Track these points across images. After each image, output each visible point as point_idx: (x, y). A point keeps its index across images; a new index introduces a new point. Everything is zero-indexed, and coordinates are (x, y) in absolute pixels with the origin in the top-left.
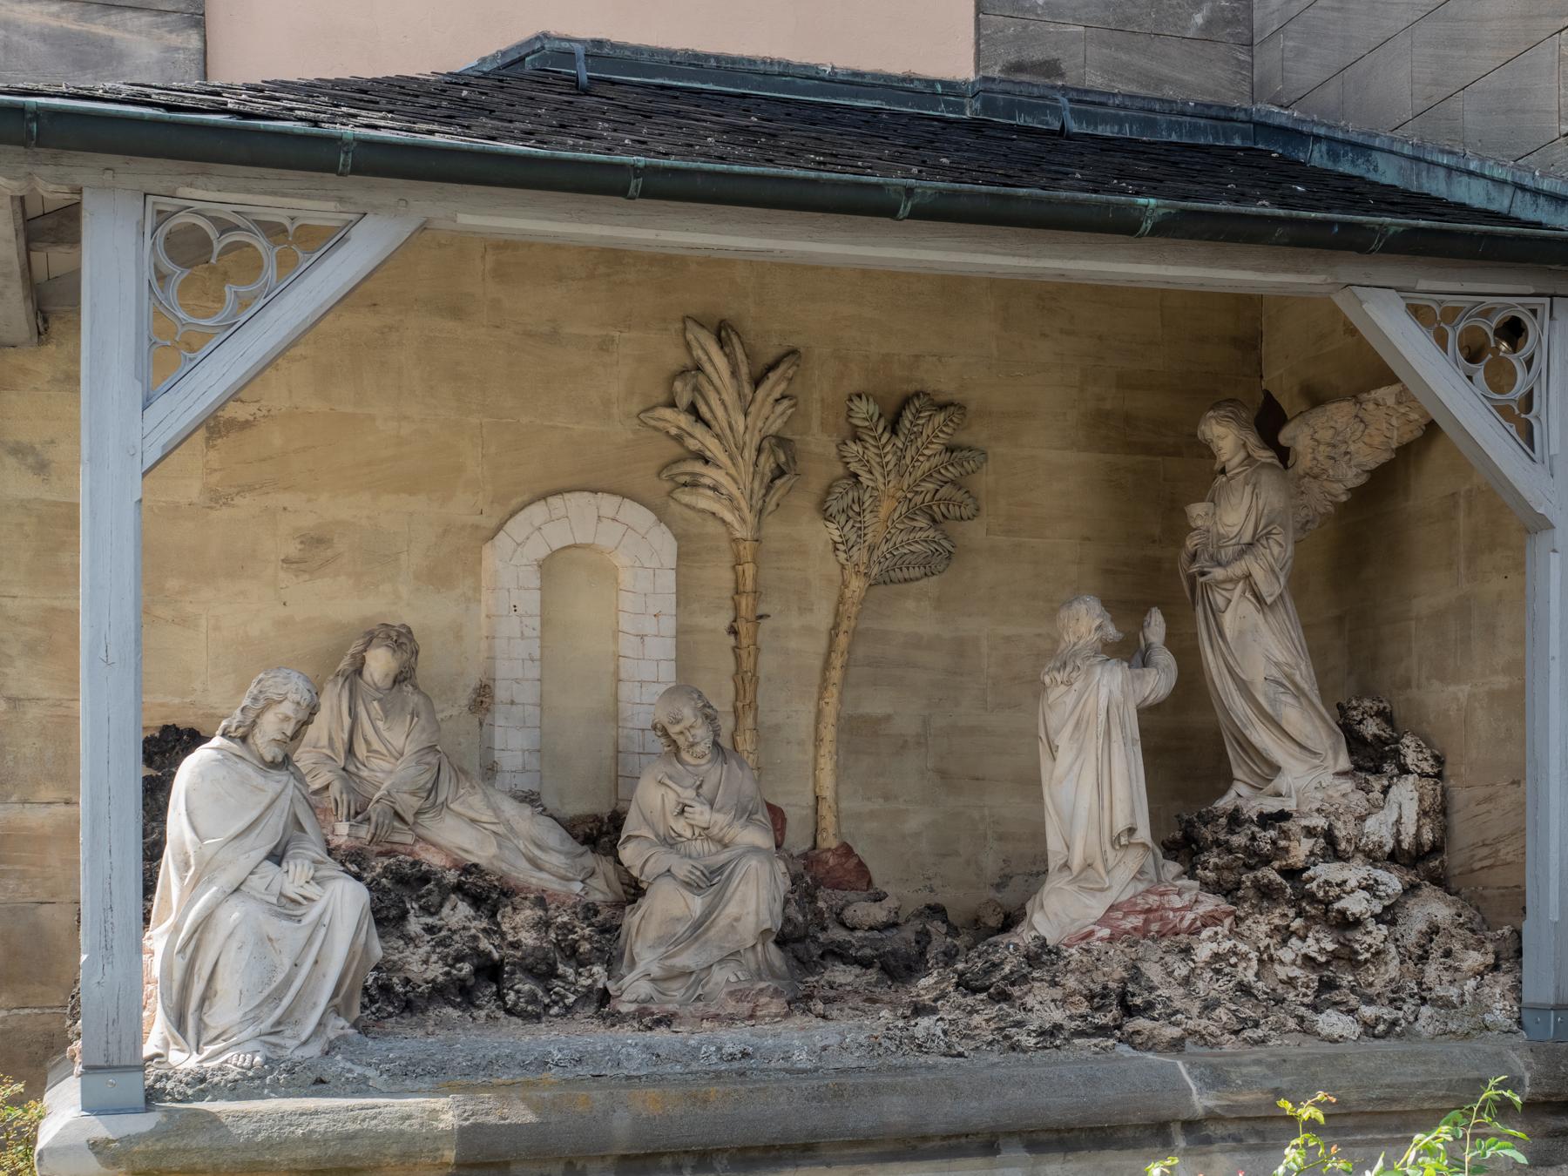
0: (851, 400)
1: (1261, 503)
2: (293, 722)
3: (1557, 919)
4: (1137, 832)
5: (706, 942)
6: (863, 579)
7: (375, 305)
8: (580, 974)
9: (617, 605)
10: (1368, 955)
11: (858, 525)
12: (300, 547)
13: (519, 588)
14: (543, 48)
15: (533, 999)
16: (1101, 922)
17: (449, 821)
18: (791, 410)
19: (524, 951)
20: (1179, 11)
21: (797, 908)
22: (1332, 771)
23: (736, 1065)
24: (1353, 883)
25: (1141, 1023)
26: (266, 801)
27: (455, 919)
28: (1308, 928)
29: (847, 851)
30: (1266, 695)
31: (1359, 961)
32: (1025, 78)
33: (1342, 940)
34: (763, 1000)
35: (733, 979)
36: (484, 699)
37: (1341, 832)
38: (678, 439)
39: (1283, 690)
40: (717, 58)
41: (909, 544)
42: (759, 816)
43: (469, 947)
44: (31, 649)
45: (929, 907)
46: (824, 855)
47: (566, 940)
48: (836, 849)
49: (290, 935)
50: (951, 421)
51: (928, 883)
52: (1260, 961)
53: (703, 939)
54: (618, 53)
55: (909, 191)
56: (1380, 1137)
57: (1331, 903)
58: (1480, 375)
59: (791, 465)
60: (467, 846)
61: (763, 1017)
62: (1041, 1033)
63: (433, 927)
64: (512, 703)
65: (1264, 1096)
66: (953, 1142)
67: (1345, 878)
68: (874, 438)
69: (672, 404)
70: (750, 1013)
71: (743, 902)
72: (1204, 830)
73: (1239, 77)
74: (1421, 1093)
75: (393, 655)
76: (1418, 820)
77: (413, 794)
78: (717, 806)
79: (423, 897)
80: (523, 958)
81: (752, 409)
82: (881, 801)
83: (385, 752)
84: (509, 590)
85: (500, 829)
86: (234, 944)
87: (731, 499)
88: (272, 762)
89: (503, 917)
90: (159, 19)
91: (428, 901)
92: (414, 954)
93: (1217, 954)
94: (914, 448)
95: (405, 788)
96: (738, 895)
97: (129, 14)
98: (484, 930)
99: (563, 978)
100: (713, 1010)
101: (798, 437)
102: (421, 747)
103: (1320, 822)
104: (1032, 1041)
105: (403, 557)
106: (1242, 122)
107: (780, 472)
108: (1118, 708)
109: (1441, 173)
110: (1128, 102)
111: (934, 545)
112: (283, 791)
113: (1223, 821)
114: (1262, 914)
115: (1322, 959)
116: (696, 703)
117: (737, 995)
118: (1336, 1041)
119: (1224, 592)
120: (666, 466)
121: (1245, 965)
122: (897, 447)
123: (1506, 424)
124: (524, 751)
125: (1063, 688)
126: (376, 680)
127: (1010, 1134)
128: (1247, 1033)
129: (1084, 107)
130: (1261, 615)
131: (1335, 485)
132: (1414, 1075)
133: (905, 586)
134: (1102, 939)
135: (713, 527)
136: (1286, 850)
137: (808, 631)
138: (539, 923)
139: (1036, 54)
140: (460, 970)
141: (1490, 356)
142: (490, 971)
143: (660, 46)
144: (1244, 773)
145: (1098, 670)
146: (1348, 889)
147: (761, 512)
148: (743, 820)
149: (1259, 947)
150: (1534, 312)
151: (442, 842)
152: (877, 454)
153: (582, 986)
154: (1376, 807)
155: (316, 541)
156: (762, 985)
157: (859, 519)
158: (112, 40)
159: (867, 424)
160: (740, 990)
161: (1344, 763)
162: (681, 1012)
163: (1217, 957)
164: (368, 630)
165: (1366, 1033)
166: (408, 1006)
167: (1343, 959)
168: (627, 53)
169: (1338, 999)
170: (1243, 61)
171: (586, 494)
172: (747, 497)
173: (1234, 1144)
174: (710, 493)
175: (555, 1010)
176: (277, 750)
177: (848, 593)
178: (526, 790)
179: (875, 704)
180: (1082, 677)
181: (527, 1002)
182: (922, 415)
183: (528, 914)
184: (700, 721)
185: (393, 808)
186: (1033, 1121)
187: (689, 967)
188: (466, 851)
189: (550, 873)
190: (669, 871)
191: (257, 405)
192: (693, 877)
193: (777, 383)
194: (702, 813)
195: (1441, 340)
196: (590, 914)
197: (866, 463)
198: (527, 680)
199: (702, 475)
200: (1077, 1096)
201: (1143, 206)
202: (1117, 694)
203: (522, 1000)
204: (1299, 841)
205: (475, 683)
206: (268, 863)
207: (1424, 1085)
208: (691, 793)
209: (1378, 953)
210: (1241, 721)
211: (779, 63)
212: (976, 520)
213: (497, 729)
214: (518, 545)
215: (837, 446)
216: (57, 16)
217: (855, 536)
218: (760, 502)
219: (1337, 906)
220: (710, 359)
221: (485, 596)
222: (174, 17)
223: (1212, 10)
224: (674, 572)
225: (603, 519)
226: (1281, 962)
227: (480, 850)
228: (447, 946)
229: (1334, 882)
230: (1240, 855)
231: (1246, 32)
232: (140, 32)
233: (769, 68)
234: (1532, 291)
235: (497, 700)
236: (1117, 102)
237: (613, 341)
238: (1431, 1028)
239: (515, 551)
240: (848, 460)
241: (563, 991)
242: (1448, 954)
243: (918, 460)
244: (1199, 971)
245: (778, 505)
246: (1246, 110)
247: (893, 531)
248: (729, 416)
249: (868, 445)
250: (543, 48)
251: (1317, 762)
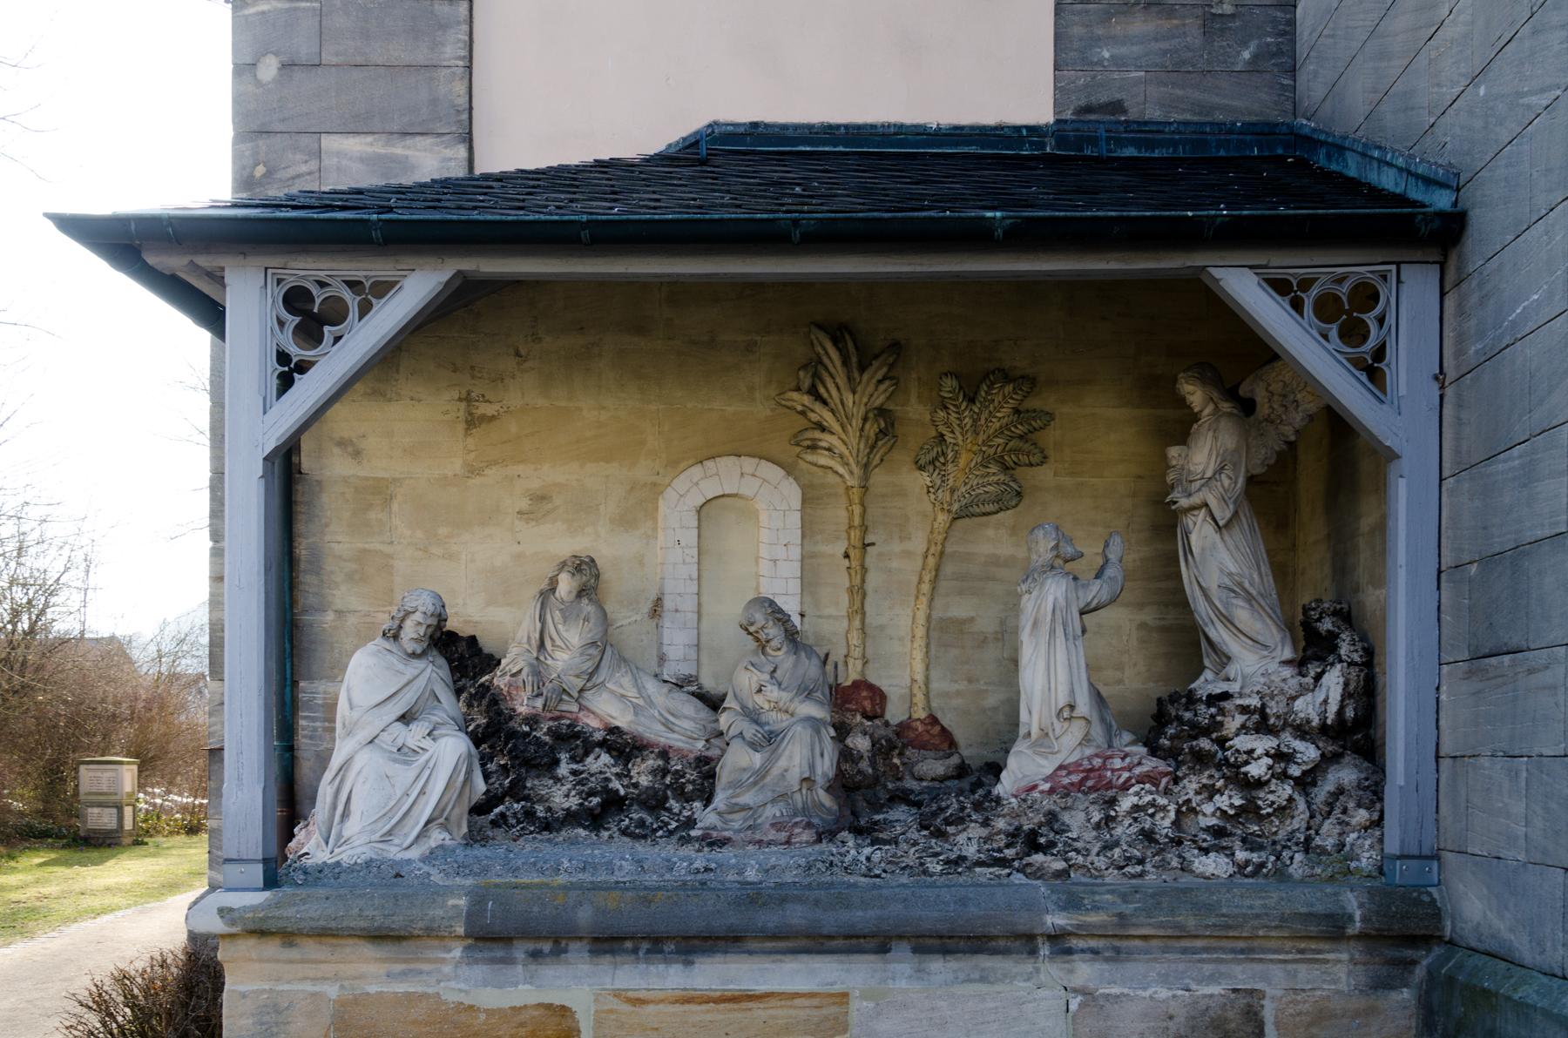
1: (1219, 445)
2: (425, 626)
3: (1402, 784)
4: (1077, 708)
6: (946, 514)
8: (684, 808)
10: (1270, 810)
12: (530, 502)
13: (681, 528)
14: (713, 132)
16: (1046, 780)
17: (605, 695)
20: (1228, 50)
22: (1278, 660)
23: (699, 877)
24: (1259, 752)
25: (1038, 858)
26: (404, 680)
29: (933, 720)
30: (1221, 601)
31: (1262, 815)
32: (1093, 117)
34: (797, 830)
35: (778, 814)
38: (803, 413)
40: (846, 127)
42: (819, 694)
44: (350, 577)
46: (914, 724)
47: (676, 783)
49: (404, 775)
50: (1021, 389)
51: (1004, 746)
52: (1178, 812)
53: (761, 784)
54: (770, 131)
55: (795, 222)
56: (1224, 956)
58: (1334, 333)
60: (614, 714)
61: (796, 843)
62: (948, 862)
64: (677, 611)
65: (1109, 919)
66: (854, 941)
68: (955, 406)
69: (798, 389)
71: (791, 757)
72: (1169, 707)
73: (1283, 98)
74: (1256, 923)
77: (577, 676)
78: (783, 686)
79: (572, 749)
80: (639, 795)
81: (859, 389)
82: (965, 683)
83: (564, 646)
86: (361, 779)
87: (841, 457)
88: (414, 653)
89: (633, 765)
90: (438, 140)
93: (1137, 806)
95: (571, 672)
96: (787, 753)
97: (419, 138)
98: (617, 774)
99: (669, 810)
100: (758, 837)
103: (1254, 702)
104: (939, 868)
105: (602, 508)
106: (1284, 134)
107: (882, 433)
108: (1062, 612)
109: (1375, 165)
110: (1182, 128)
112: (418, 676)
115: (1231, 812)
117: (777, 826)
118: (1208, 878)
121: (1162, 815)
123: (1357, 373)
125: (1027, 596)
127: (901, 937)
128: (1128, 869)
129: (1143, 136)
131: (1286, 428)
132: (1251, 907)
133: (984, 519)
134: (1042, 792)
136: (1221, 724)
137: (908, 554)
139: (1103, 97)
140: (590, 802)
142: (613, 804)
143: (802, 121)
144: (1211, 662)
145: (1049, 581)
146: (1255, 756)
148: (801, 698)
150: (1384, 278)
151: (598, 711)
154: (1303, 690)
155: (540, 498)
156: (798, 819)
158: (407, 157)
161: (1288, 653)
165: (1239, 872)
166: (547, 826)
168: (777, 130)
169: (1225, 844)
170: (1287, 85)
172: (854, 455)
173: (1091, 956)
174: (826, 453)
176: (415, 645)
177: (936, 526)
179: (960, 609)
180: (1037, 588)
181: (636, 827)
184: (771, 623)
186: (908, 928)
190: (741, 733)
191: (501, 404)
193: (879, 368)
194: (771, 691)
195: (1297, 305)
196: (701, 764)
197: (948, 425)
199: (820, 440)
200: (947, 911)
201: (991, 218)
204: (1233, 717)
206: (398, 724)
207: (1257, 916)
208: (767, 677)
210: (1203, 620)
211: (895, 125)
212: (1045, 466)
216: (371, 144)
218: (865, 459)
219: (1243, 770)
221: (660, 534)
222: (448, 137)
223: (1258, 46)
226: (1204, 815)
227: (623, 720)
228: (583, 785)
231: (1289, 61)
232: (425, 150)
233: (886, 131)
235: (665, 609)
236: (1172, 129)
238: (1300, 871)
239: (679, 500)
242: (1345, 811)
244: (1120, 819)
245: (882, 460)
246: (1288, 125)
250: (713, 132)
251: (1266, 653)
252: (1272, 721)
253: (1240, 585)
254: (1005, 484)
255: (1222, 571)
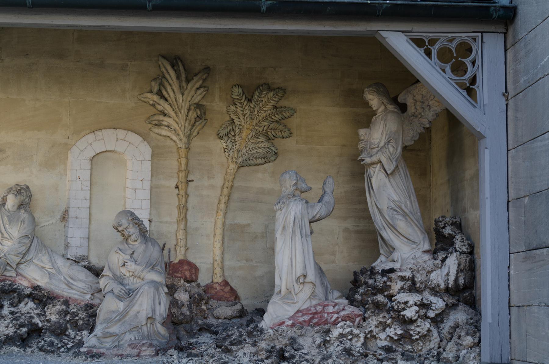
0: (232, 88)
3: (491, 321)
5: (124, 322)
6: (235, 164)
7: (27, 55)
8: (77, 335)
9: (126, 176)
10: (417, 337)
11: (233, 141)
15: (51, 344)
17: (32, 267)
18: (205, 92)
19: (51, 324)
21: (187, 308)
22: (421, 250)
24: (411, 303)
27: (25, 309)
28: (393, 323)
30: (389, 216)
31: (413, 340)
33: (405, 329)
34: (144, 348)
36: (65, 216)
37: (419, 278)
38: (153, 105)
39: (396, 213)
41: (256, 149)
43: (27, 321)
45: (256, 309)
48: (221, 283)
50: (277, 95)
53: (123, 321)
57: (400, 312)
58: (448, 69)
59: (203, 116)
63: (13, 312)
64: (77, 218)
67: (408, 300)
69: (151, 92)
70: (137, 354)
71: (141, 305)
72: (361, 276)
75: (15, 197)
76: (457, 274)
77: (16, 255)
80: (50, 327)
82: (245, 261)
83: (9, 238)
84: (77, 170)
85: (53, 271)
87: (175, 131)
89: (48, 309)
91: (13, 301)
92: (3, 323)
93: (342, 334)
94: (258, 107)
95: (12, 253)
96: (139, 302)
99: (68, 336)
100: (120, 352)
101: (208, 104)
102: (21, 236)
103: (408, 274)
107: (199, 117)
108: (299, 221)
111: (268, 149)
113: (369, 273)
114: (375, 316)
116: (129, 218)
117: (132, 345)
119: (373, 169)
120: (149, 118)
121: (356, 339)
122: (251, 107)
124: (81, 238)
125: (279, 212)
126: (9, 208)
130: (387, 179)
133: (257, 167)
135: (169, 143)
136: (390, 287)
138: (61, 311)
141: (454, 60)
145: (292, 203)
146: (409, 305)
147: (189, 136)
148: (148, 269)
149: (365, 332)
150: (475, 40)
151: (27, 276)
152: (242, 110)
153: (77, 340)
154: (435, 268)
156: (144, 342)
157: (234, 138)
159: (238, 97)
160: (134, 344)
162: (106, 353)
163: (341, 335)
164: (10, 187)
167: (407, 338)
169: (392, 357)
171: (112, 129)
172: (182, 130)
174: (166, 128)
175: (62, 350)
177: (229, 171)
178: (81, 255)
180: (285, 207)
181: (48, 346)
182: (263, 93)
183: (59, 307)
184: (131, 225)
185: (6, 261)
187: (116, 333)
188: (36, 280)
189: (76, 290)
190: (112, 290)
192: (121, 293)
193: (197, 81)
194: (131, 265)
195: (428, 53)
197: (236, 114)
198: (83, 208)
199: (163, 121)
202: (299, 215)
203: (46, 345)
204: (396, 283)
205: (63, 209)
208: (128, 257)
209: (424, 336)
210: (379, 227)
213: (69, 229)
214: (81, 151)
215: (226, 107)
217: (231, 145)
218: (189, 132)
220: (168, 72)
221: (68, 173)
224: (150, 162)
225: (119, 140)
226: (380, 339)
227: (42, 281)
228: (17, 320)
229: (401, 302)
230: (370, 289)
234: (472, 30)
235: (70, 216)
237: (128, 66)
239: (80, 154)
240: (230, 113)
241: (66, 341)
243: (261, 113)
245: (198, 133)
247: (248, 143)
248: (176, 95)
249: (237, 107)
251: (414, 246)
252: (418, 285)
253: (400, 207)
254: (268, 148)
255: (389, 199)
